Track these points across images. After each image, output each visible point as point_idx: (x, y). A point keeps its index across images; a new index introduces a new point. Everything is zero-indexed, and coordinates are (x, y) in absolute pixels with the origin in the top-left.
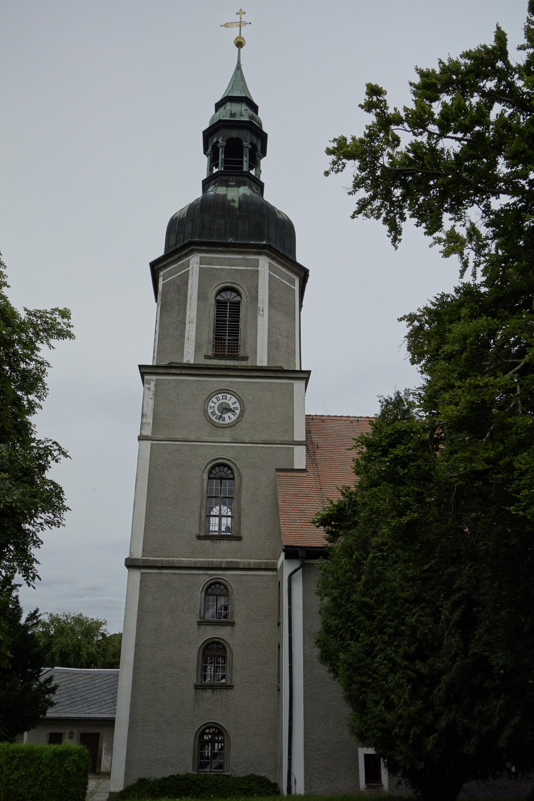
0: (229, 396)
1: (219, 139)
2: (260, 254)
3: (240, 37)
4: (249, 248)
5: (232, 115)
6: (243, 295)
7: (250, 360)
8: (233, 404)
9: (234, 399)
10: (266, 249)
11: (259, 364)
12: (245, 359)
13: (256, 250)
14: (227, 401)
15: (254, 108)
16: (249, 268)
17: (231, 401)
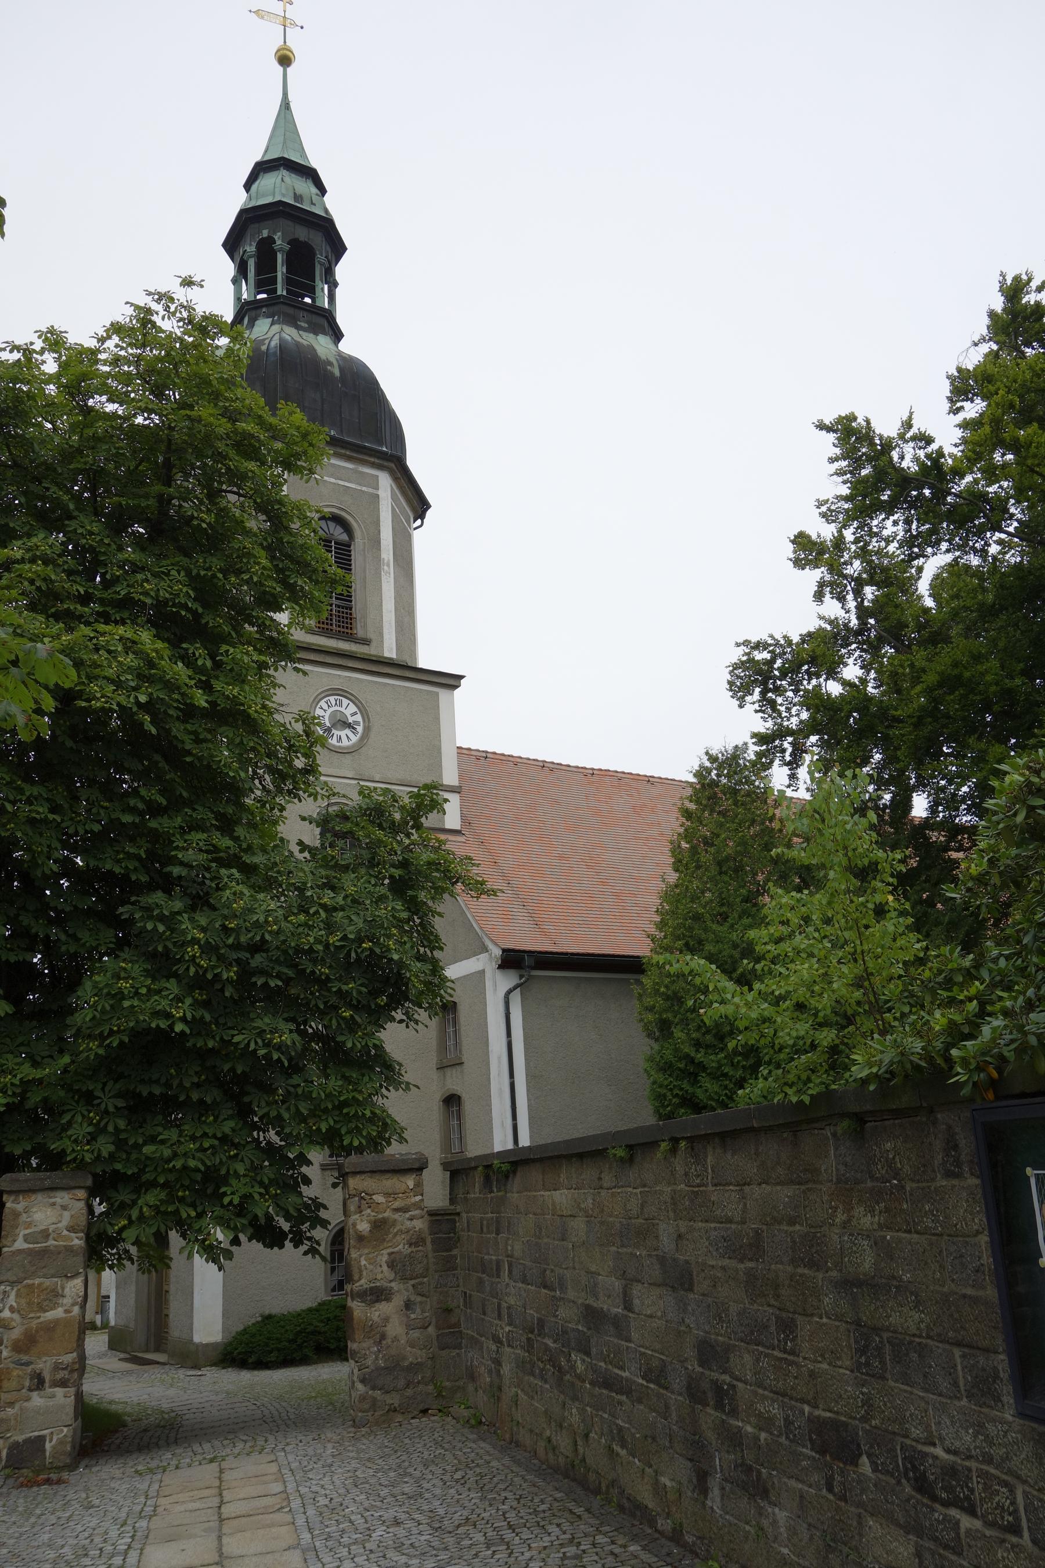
0: (345, 701)
1: (275, 233)
2: (380, 467)
3: (285, 47)
4: (365, 454)
5: (298, 197)
6: (358, 534)
7: (374, 644)
8: (353, 714)
9: (353, 708)
10: (392, 461)
11: (387, 654)
12: (366, 642)
13: (377, 461)
14: (342, 709)
15: (323, 191)
16: (364, 489)
17: (349, 709)
